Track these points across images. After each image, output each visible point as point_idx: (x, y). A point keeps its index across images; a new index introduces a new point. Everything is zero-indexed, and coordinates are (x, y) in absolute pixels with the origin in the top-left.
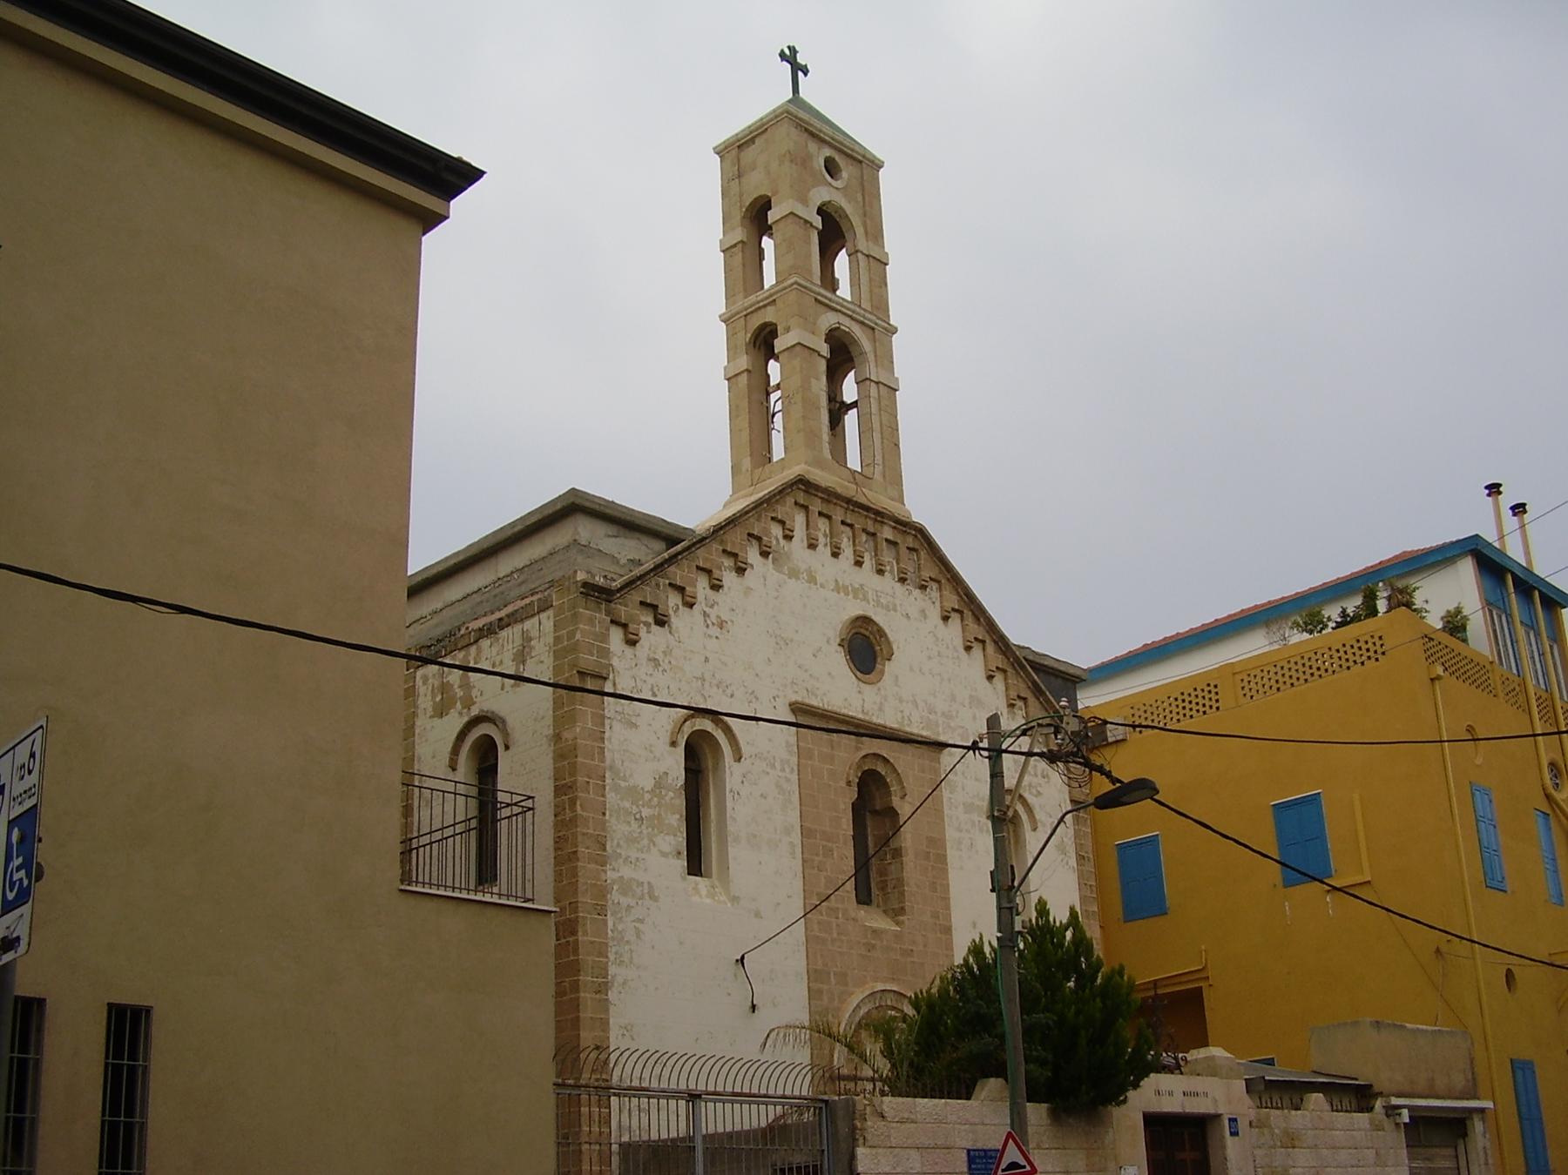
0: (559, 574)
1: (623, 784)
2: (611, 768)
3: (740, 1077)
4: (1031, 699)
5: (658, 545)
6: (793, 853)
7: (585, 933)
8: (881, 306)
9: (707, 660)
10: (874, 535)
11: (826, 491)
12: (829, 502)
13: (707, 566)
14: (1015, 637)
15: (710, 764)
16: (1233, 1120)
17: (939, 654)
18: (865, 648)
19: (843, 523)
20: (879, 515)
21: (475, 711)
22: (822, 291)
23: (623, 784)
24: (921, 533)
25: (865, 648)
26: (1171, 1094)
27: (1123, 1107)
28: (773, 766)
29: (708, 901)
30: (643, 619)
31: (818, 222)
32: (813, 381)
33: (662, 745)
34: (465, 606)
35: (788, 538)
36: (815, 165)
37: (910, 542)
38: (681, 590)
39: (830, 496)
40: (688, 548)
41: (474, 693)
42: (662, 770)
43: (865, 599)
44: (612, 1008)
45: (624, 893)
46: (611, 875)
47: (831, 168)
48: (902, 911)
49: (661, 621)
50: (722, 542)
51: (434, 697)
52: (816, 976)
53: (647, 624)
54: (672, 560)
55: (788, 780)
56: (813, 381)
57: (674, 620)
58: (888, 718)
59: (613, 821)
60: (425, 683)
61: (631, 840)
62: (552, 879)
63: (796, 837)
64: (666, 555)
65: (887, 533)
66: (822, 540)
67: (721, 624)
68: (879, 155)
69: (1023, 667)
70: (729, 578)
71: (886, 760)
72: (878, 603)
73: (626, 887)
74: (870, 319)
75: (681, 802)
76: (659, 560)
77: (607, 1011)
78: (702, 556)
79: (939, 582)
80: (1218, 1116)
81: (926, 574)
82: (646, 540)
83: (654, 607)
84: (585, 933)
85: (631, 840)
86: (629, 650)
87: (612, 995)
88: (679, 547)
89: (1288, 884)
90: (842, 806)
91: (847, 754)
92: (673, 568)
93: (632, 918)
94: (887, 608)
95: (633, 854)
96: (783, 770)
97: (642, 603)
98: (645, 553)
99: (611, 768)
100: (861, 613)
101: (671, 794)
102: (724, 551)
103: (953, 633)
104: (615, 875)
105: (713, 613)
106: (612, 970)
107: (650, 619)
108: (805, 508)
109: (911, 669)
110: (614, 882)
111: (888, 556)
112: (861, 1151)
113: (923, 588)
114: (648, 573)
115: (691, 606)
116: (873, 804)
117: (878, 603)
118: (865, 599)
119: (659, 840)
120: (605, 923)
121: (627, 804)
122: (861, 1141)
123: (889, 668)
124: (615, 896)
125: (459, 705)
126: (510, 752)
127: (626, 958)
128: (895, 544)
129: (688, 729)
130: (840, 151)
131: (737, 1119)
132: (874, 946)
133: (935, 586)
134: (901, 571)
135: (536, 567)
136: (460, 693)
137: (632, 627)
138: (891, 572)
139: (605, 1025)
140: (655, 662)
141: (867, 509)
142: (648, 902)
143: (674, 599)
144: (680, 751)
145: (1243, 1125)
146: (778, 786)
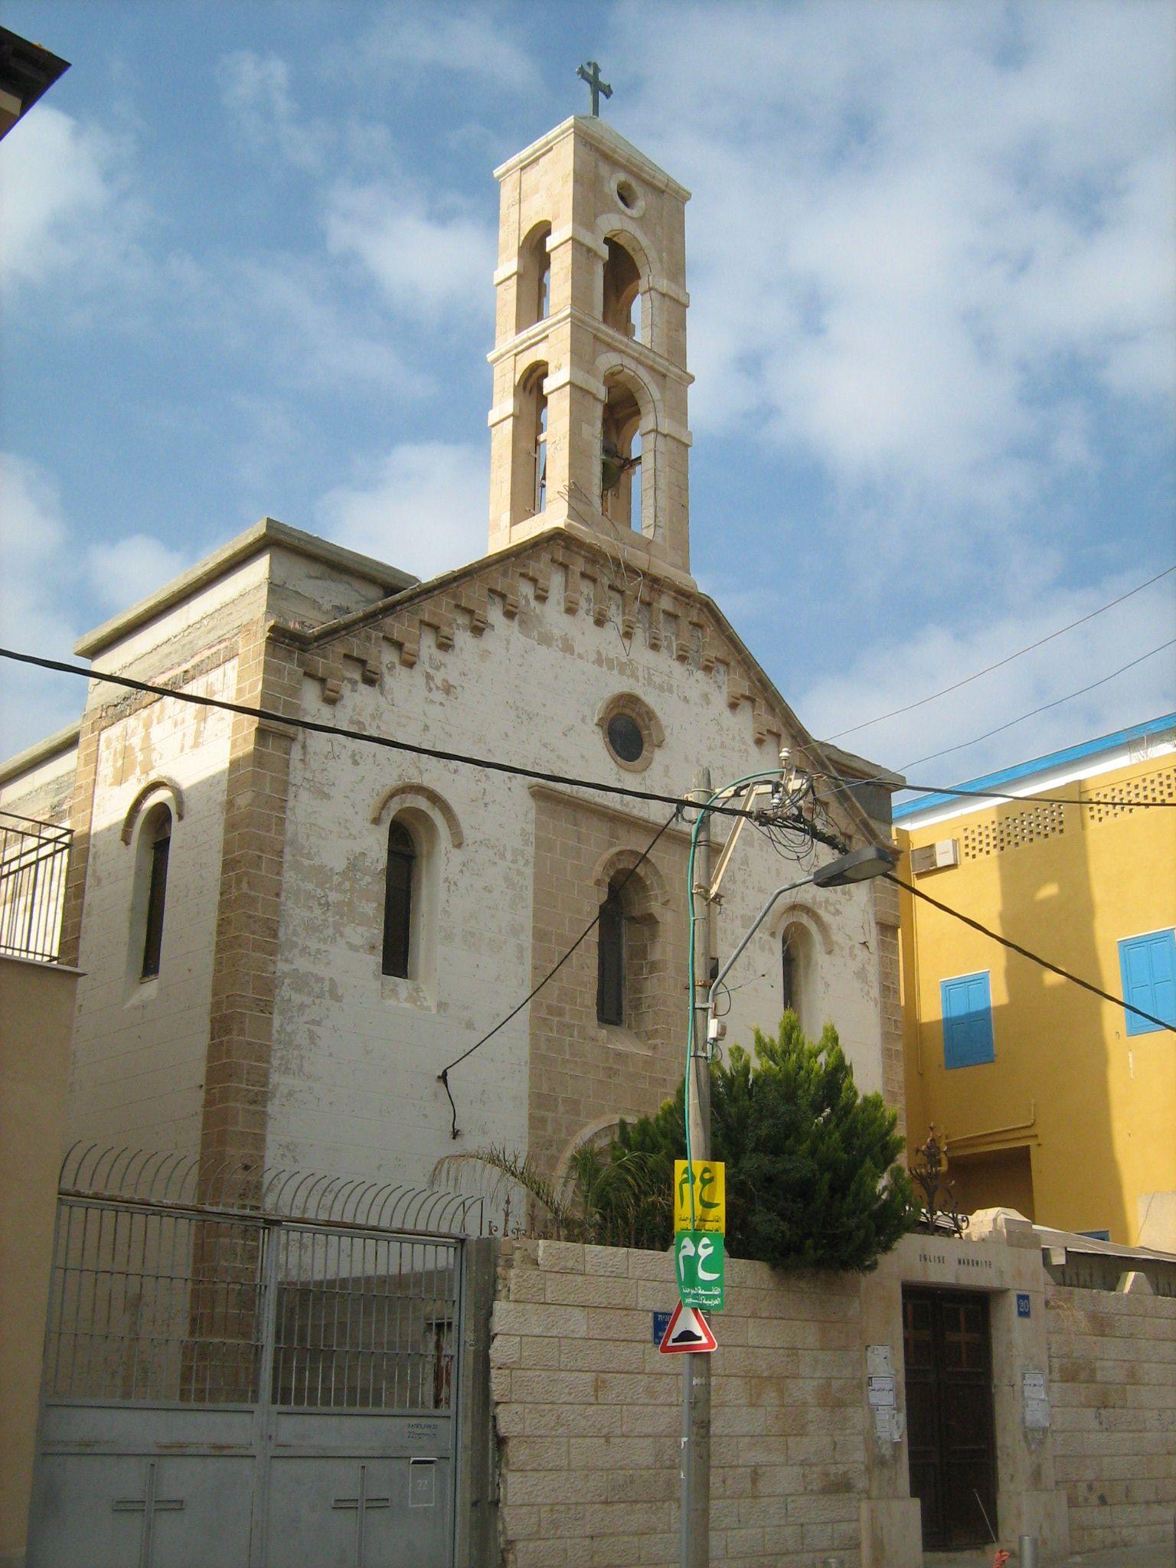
0: (245, 620)
1: (307, 862)
3: (427, 1207)
5: (373, 592)
7: (242, 1032)
8: (677, 352)
9: (426, 728)
10: (649, 604)
13: (435, 621)
14: (818, 731)
15: (425, 852)
16: (1022, 1298)
17: (723, 746)
18: (628, 732)
19: (611, 587)
20: (656, 583)
21: (153, 776)
22: (603, 327)
23: (307, 862)
24: (708, 607)
25: (628, 732)
26: (941, 1260)
27: (876, 1272)
28: (503, 856)
29: (407, 1005)
30: (348, 675)
31: (604, 251)
32: (584, 426)
33: (361, 820)
34: (154, 659)
35: (542, 598)
36: (606, 190)
37: (694, 616)
38: (399, 646)
40: (410, 598)
41: (155, 756)
42: (358, 850)
43: (634, 676)
44: (271, 1124)
45: (298, 989)
46: (282, 967)
47: (625, 196)
49: (370, 680)
50: (454, 597)
51: (115, 761)
52: (540, 1101)
53: (354, 683)
54: (388, 610)
55: (519, 873)
56: (584, 426)
57: (388, 680)
59: (290, 904)
60: (108, 747)
61: (312, 928)
62: (211, 968)
63: (527, 940)
64: (380, 604)
65: (665, 603)
66: (583, 605)
67: (448, 689)
69: (824, 767)
70: (463, 638)
72: (650, 681)
73: (301, 982)
74: (662, 364)
75: (380, 888)
76: (371, 608)
77: (263, 1125)
78: (427, 610)
79: (727, 664)
80: (1002, 1293)
81: (712, 654)
82: (357, 584)
83: (363, 662)
84: (242, 1032)
85: (312, 928)
87: (272, 1108)
88: (397, 596)
89: (1133, 1032)
90: (587, 908)
92: (389, 620)
93: (305, 1018)
94: (661, 688)
95: (313, 945)
96: (514, 861)
97: (346, 656)
98: (356, 600)
99: (292, 843)
100: (626, 690)
101: (368, 879)
102: (457, 606)
103: (744, 724)
105: (439, 677)
106: (275, 1078)
107: (357, 676)
108: (565, 567)
109: (686, 759)
110: (285, 975)
111: (665, 631)
112: (499, 1306)
113: (707, 669)
114: (355, 622)
116: (623, 912)
117: (650, 681)
118: (634, 676)
119: (348, 930)
121: (310, 886)
122: (504, 1293)
123: (658, 756)
124: (285, 992)
125: (138, 771)
126: (183, 822)
127: (294, 1066)
128: (675, 617)
129: (395, 806)
130: (638, 177)
131: (333, 1252)
132: (616, 1072)
133: (722, 668)
134: (681, 648)
135: (226, 611)
136: (140, 757)
137: (331, 683)
138: (669, 648)
139: (259, 1141)
143: (389, 656)
144: (383, 834)
145: (1037, 1304)
146: (507, 879)
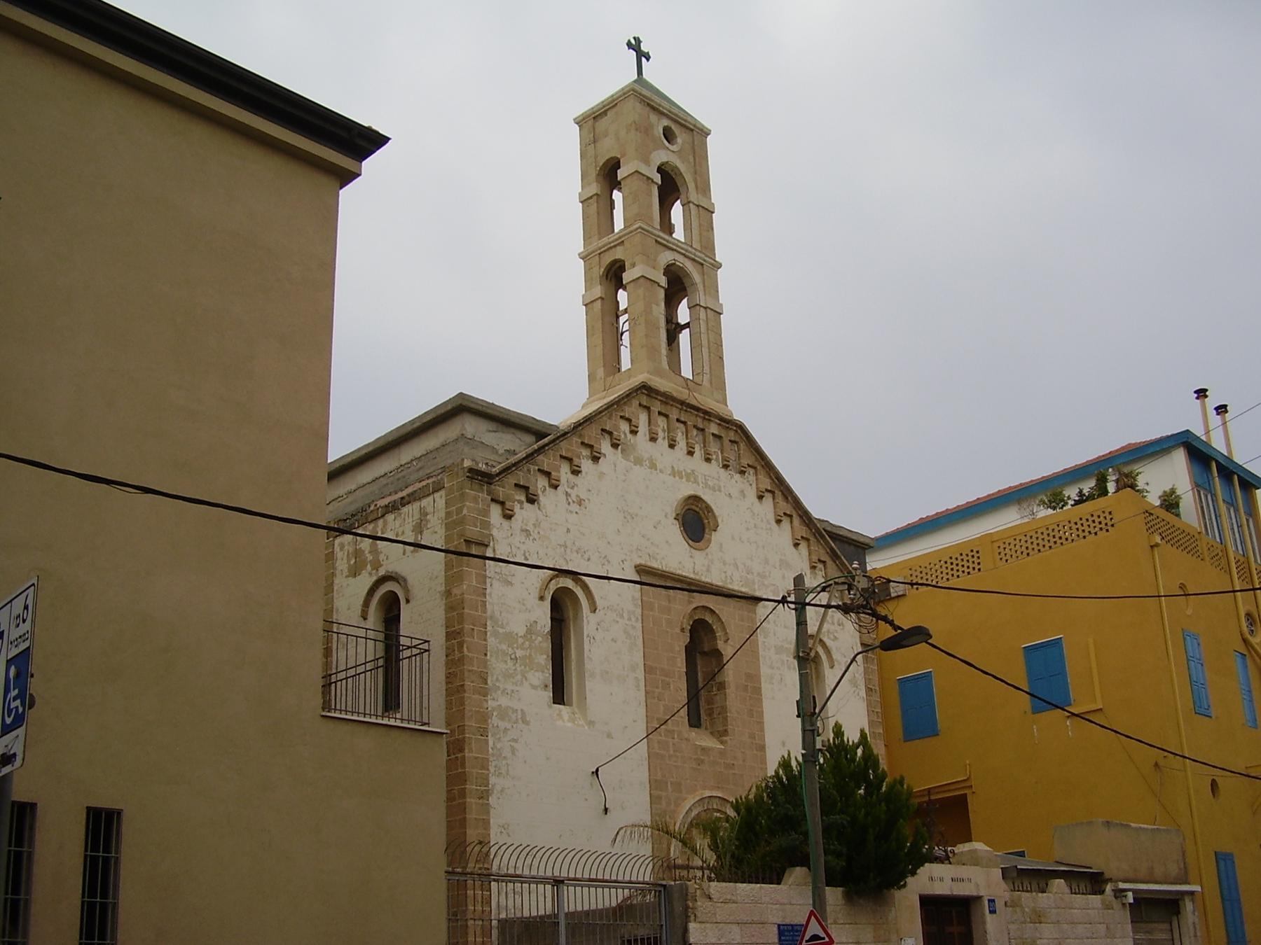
0: (449, 462)
1: (501, 631)
2: (491, 618)
3: (595, 866)
4: (829, 563)
5: (529, 439)
6: (638, 686)
7: (471, 751)
8: (709, 246)
9: (568, 531)
10: (703, 430)
11: (664, 395)
12: (666, 403)
13: (569, 455)
14: (816, 512)
15: (571, 614)
16: (991, 901)
17: (755, 526)
18: (695, 521)
19: (678, 420)
20: (707, 415)
21: (382, 572)
22: (661, 234)
23: (501, 631)
24: (741, 428)
25: (695, 521)
26: (941, 879)
27: (903, 890)
28: (622, 616)
29: (570, 724)
30: (517, 498)
31: (658, 178)
32: (654, 306)
33: (533, 599)
34: (374, 487)
35: (634, 432)
36: (656, 132)
37: (732, 436)
38: (548, 474)
39: (667, 399)
40: (554, 441)
41: (382, 557)
42: (532, 619)
43: (696, 481)
44: (492, 811)
45: (502, 718)
46: (491, 704)
47: (668, 135)
48: (725, 732)
49: (532, 500)
50: (580, 436)
51: (349, 560)
52: (656, 785)
53: (520, 502)
54: (540, 450)
55: (634, 627)
56: (654, 306)
57: (542, 498)
58: (714, 578)
59: (493, 660)
60: (341, 549)
61: (508, 676)
62: (444, 707)
63: (640, 673)
64: (535, 447)
65: (714, 428)
66: (661, 434)
67: (580, 502)
68: (707, 125)
69: (823, 537)
70: (586, 465)
71: (712, 612)
72: (706, 485)
73: (504, 713)
74: (700, 256)
75: (548, 645)
76: (530, 450)
77: (488, 813)
78: (564, 447)
79: (755, 468)
80: (979, 898)
81: (745, 462)
82: (519, 434)
83: (526, 488)
84: (471, 751)
85: (508, 676)
86: (506, 523)
87: (492, 801)
88: (546, 440)
89: (1036, 711)
90: (677, 649)
91: (681, 607)
92: (541, 457)
93: (508, 738)
94: (714, 489)
95: (509, 687)
96: (630, 619)
97: (516, 485)
98: (519, 444)
99: (491, 618)
100: (692, 493)
101: (540, 639)
102: (582, 443)
103: (767, 509)
104: (494, 704)
105: (573, 493)
106: (492, 780)
107: (523, 498)
108: (648, 408)
109: (733, 538)
110: (494, 709)
111: (714, 447)
112: (692, 926)
113: (742, 473)
114: (521, 461)
115: (556, 487)
116: (702, 646)
117: (706, 485)
118: (696, 481)
119: (530, 675)
120: (487, 742)
121: (504, 647)
122: (692, 918)
123: (715, 537)
124: (495, 721)
125: (369, 567)
126: (410, 605)
127: (503, 771)
128: (719, 437)
129: (553, 586)
130: (676, 121)
131: (593, 900)
132: (703, 761)
133: (752, 471)
134: (724, 459)
135: (431, 456)
136: (370, 557)
137: (508, 504)
138: (717, 460)
139: (486, 824)
140: (527, 532)
141: (698, 409)
142: (521, 725)
143: (542, 482)
144: (547, 604)
145: (999, 905)
146: (625, 632)
